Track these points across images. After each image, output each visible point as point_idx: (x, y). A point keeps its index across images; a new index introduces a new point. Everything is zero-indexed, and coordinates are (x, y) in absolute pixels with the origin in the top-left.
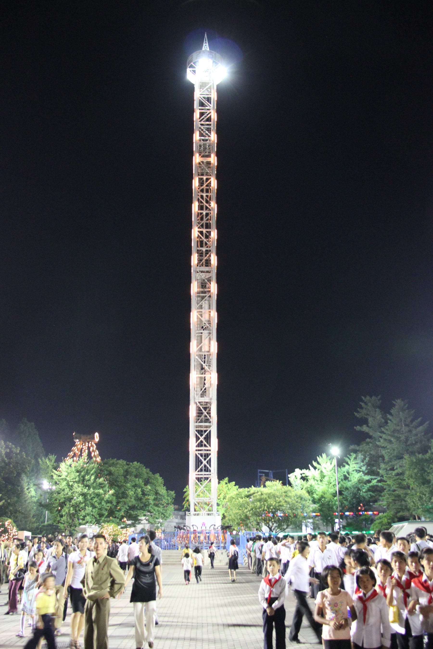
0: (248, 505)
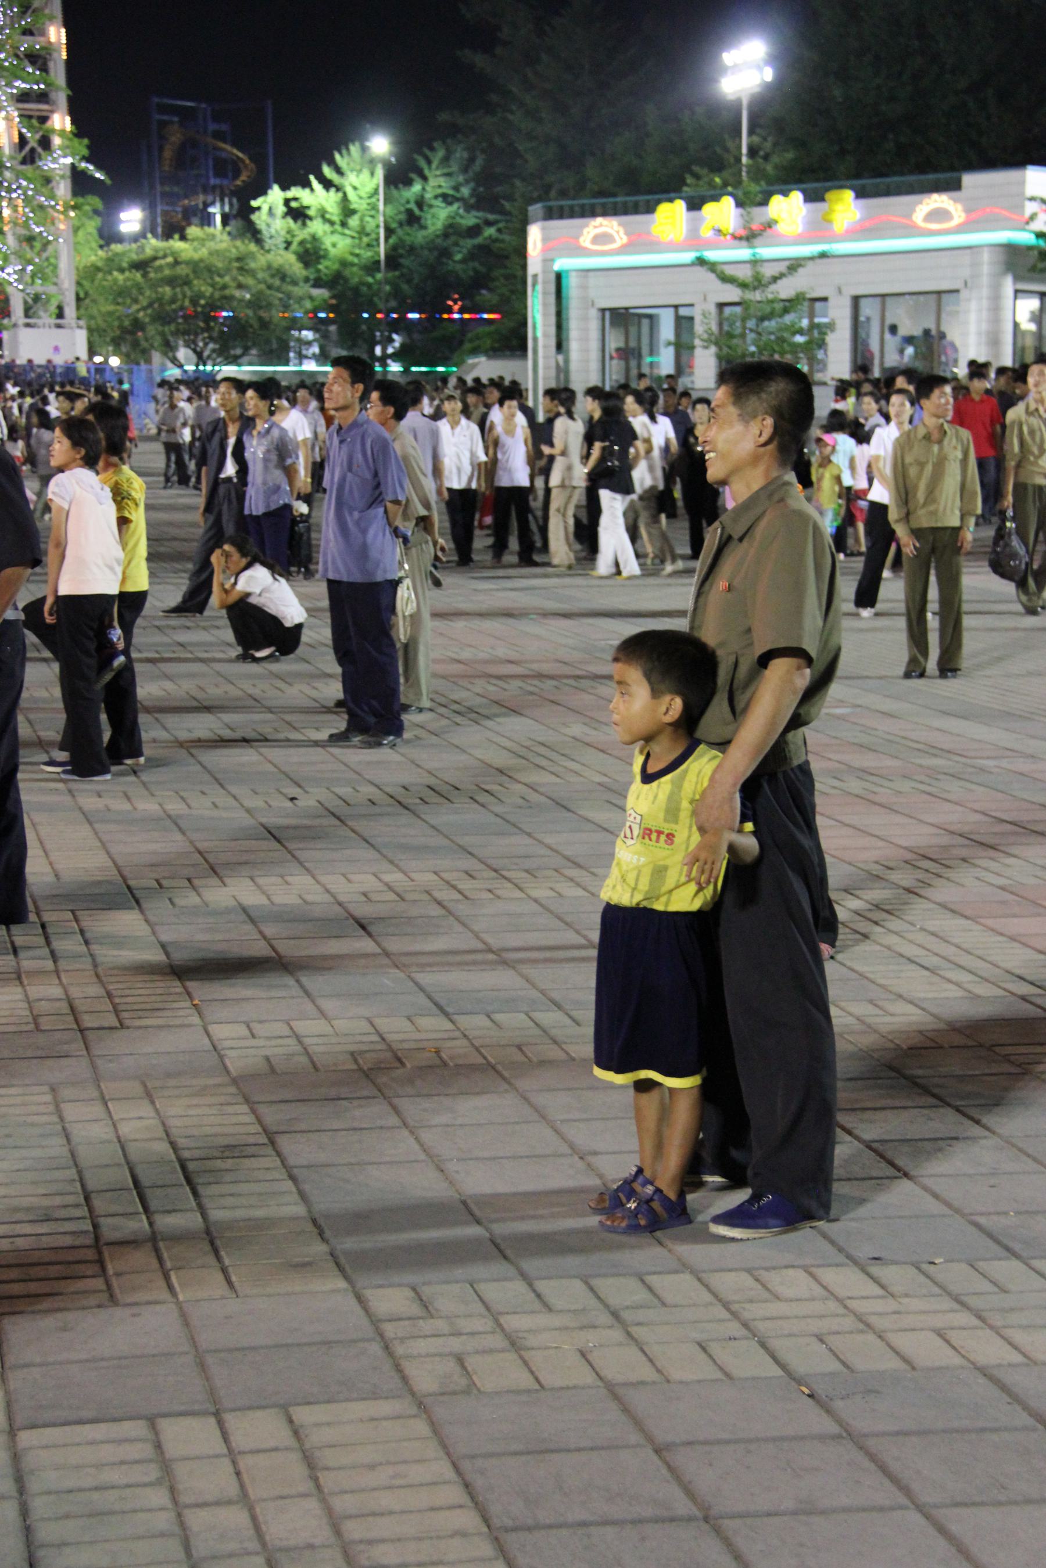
0: (141, 294)
